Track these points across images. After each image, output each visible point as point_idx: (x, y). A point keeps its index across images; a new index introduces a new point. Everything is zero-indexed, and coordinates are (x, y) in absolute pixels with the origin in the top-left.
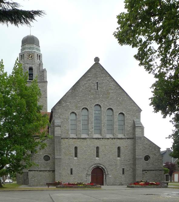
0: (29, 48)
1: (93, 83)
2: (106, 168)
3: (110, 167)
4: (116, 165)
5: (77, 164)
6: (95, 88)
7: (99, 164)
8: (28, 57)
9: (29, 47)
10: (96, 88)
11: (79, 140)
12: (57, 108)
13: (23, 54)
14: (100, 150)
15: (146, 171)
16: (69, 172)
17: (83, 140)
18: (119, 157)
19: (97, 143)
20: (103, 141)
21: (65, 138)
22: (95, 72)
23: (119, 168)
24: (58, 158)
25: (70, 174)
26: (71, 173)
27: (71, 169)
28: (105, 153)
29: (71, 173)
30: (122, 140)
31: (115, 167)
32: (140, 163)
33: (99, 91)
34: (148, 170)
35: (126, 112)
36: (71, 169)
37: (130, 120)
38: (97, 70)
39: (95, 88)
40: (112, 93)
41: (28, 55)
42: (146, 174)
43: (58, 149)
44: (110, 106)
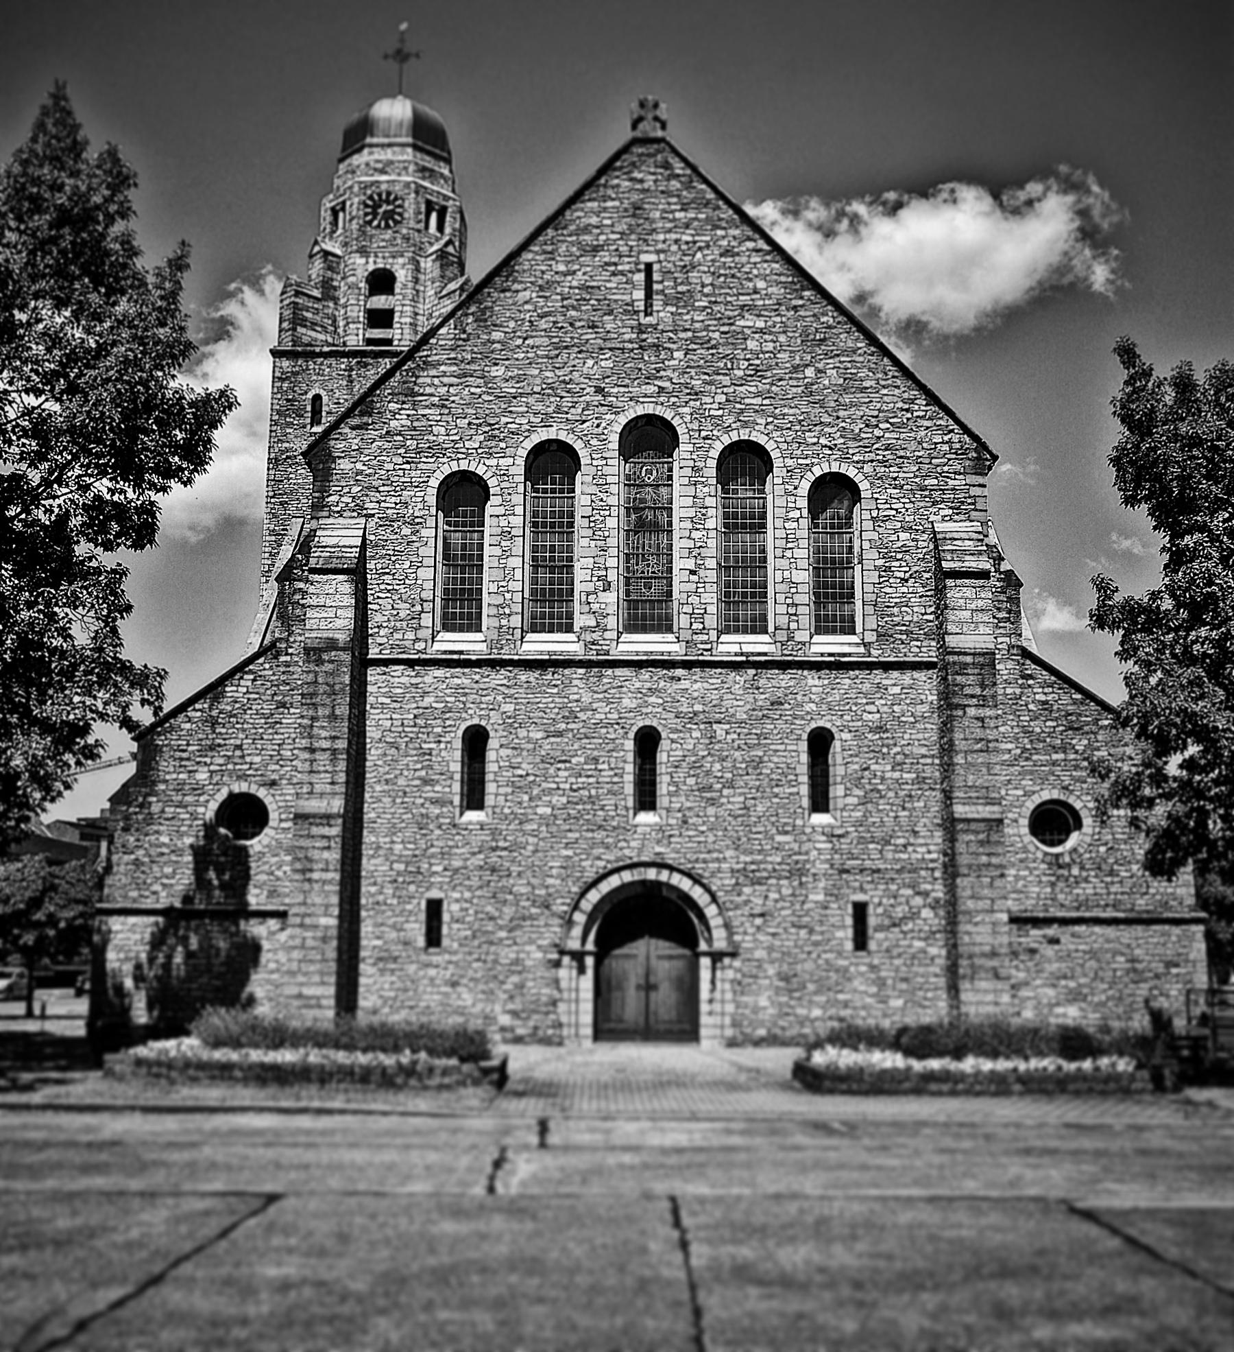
0: (379, 166)
1: (622, 273)
2: (714, 899)
3: (747, 890)
4: (798, 872)
5: (478, 860)
6: (632, 303)
7: (661, 866)
8: (366, 214)
9: (378, 161)
10: (641, 305)
11: (499, 678)
12: (341, 445)
13: (344, 203)
14: (494, 754)
15: (1051, 931)
16: (417, 931)
17: (532, 676)
18: (825, 809)
19: (634, 700)
20: (694, 684)
21: (479, 664)
22: (635, 197)
23: (821, 897)
24: (314, 816)
25: (421, 941)
26: (433, 938)
27: (434, 909)
28: (705, 781)
29: (433, 938)
30: (846, 680)
31: (786, 891)
32: (984, 859)
33: (660, 320)
34: (1064, 922)
35: (868, 468)
36: (434, 909)
37: (903, 529)
38: (649, 184)
39: (632, 303)
40: (761, 331)
41: (367, 206)
42: (1049, 951)
43: (325, 744)
44: (745, 424)
